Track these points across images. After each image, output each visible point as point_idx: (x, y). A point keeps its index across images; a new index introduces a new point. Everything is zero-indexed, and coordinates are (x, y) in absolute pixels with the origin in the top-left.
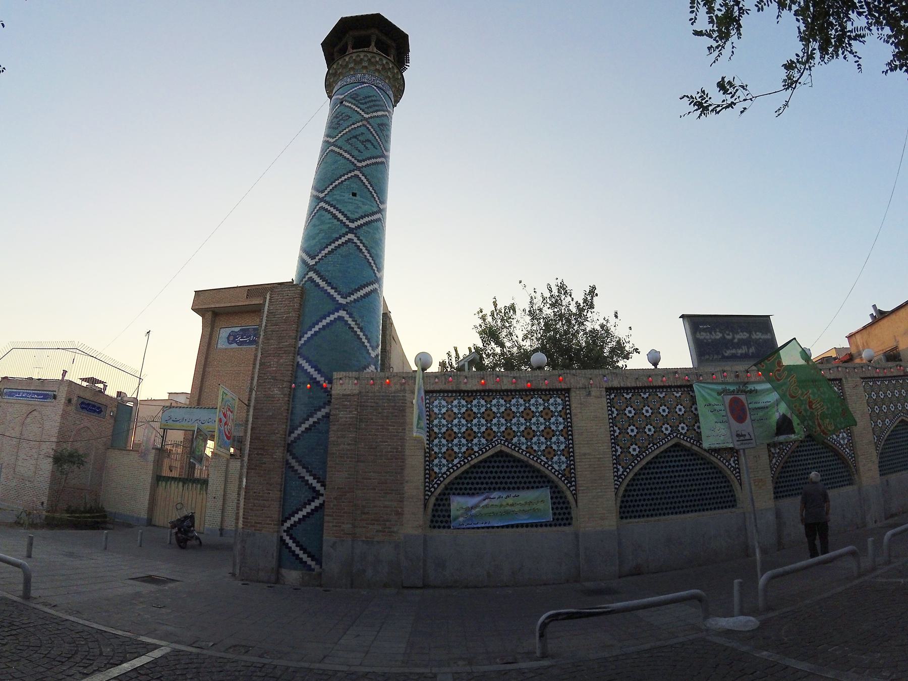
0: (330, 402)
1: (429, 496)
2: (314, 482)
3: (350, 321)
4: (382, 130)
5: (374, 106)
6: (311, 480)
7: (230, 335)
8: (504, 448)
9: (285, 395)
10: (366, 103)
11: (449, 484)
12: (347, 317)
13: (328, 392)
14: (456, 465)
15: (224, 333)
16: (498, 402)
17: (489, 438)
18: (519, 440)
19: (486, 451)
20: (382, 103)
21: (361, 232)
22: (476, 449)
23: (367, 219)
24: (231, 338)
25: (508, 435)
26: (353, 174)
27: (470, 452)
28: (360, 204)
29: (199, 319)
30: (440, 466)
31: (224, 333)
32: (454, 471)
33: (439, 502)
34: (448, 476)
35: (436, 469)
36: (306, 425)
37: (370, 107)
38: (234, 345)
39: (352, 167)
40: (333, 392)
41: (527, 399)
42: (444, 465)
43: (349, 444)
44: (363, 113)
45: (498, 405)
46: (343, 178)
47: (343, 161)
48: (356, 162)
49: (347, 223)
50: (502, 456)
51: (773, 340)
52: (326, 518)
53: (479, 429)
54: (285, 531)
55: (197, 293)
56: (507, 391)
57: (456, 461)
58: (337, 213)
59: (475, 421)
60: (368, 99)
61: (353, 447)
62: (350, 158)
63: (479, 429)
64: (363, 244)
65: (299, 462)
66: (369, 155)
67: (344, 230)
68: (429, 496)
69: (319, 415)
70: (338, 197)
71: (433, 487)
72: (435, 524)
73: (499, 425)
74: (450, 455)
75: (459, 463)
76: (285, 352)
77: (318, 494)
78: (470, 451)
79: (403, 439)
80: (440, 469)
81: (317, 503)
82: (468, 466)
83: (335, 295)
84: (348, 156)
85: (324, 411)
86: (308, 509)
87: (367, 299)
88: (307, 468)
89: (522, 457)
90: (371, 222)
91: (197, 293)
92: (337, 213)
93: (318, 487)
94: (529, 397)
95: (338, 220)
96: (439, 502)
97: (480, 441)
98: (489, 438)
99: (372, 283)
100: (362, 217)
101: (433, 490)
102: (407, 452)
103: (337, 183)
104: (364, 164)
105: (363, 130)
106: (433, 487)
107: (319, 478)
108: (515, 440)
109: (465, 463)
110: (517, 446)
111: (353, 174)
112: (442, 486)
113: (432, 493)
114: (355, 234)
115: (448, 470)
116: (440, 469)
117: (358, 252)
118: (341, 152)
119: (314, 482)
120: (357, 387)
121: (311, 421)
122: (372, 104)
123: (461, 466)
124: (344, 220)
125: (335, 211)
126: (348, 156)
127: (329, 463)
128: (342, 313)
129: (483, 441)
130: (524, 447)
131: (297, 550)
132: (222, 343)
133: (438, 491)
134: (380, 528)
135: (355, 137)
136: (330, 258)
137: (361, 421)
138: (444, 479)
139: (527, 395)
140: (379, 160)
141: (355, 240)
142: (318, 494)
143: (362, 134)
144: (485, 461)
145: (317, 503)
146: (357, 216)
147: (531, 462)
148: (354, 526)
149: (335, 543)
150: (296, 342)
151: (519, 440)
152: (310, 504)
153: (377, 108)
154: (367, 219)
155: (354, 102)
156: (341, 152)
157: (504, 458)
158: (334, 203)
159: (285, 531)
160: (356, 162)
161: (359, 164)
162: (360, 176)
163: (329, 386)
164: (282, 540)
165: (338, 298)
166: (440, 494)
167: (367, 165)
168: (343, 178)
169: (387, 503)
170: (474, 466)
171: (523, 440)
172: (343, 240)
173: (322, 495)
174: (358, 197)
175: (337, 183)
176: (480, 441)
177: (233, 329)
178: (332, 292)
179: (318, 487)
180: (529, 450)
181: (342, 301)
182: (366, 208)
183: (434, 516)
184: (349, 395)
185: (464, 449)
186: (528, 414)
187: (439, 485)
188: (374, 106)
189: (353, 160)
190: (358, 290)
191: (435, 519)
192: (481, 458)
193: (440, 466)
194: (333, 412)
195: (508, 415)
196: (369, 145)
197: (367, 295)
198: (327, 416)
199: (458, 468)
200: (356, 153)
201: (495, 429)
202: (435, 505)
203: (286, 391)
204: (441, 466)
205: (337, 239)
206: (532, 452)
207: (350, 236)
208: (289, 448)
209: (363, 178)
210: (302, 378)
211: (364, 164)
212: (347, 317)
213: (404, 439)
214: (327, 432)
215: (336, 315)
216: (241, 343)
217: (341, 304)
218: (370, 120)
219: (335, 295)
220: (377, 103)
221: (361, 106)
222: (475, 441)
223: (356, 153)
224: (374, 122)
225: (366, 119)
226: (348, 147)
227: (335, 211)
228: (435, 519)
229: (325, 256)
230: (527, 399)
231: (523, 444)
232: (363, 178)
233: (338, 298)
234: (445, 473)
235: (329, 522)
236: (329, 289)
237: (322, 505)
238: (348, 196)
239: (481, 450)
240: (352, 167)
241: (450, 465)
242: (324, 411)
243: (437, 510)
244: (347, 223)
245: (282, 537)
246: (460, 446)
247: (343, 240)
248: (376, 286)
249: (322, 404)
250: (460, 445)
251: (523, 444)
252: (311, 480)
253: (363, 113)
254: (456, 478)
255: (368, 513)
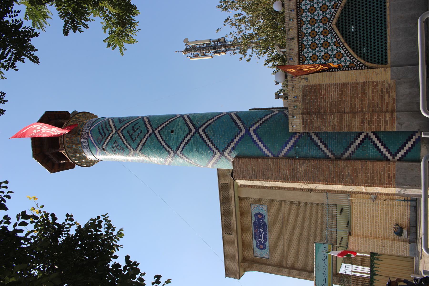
0: (308, 133)
1: (365, 66)
2: (360, 139)
3: (256, 125)
4: (124, 121)
5: (106, 127)
6: (358, 142)
7: (259, 248)
8: (334, 23)
9: (304, 163)
10: (104, 133)
11: (357, 55)
12: (254, 128)
13: (302, 135)
14: (345, 52)
15: (258, 252)
16: (305, 29)
17: (328, 32)
18: (328, 14)
19: (336, 33)
20: (100, 125)
21: (198, 125)
22: (334, 40)
23: (189, 122)
24: (261, 247)
25: (325, 21)
26: (158, 134)
27: (337, 44)
28: (179, 127)
29: (248, 275)
30: (345, 61)
31: (258, 252)
32: (349, 52)
33: (369, 60)
34: (352, 56)
35: (348, 63)
36: (323, 147)
37: (107, 130)
38: (267, 244)
39: (153, 135)
40: (302, 131)
41: (302, 11)
42: (345, 59)
43: (334, 119)
44: (112, 133)
45: (307, 29)
46: (161, 140)
47: (148, 142)
48: (149, 133)
49: (192, 134)
50: (339, 24)
51: (348, 263)
52: (383, 130)
53: (322, 39)
54: (393, 158)
55: (227, 275)
56: (298, 24)
57: (342, 52)
58: (185, 141)
59: (317, 42)
60: (101, 131)
61: (336, 116)
62: (146, 137)
63: (322, 39)
64: (203, 124)
65: (346, 150)
66: (144, 126)
67: (197, 135)
68: (365, 66)
69: (316, 139)
70: (174, 142)
71: (359, 64)
72: (384, 62)
73: (319, 27)
74: (339, 56)
75: (343, 50)
76: (277, 165)
77: (367, 136)
78: (336, 44)
79: (329, 85)
80: (348, 61)
81: (373, 137)
82: (345, 44)
83: (240, 136)
84: (145, 139)
85: (314, 136)
86: (377, 142)
87: (242, 118)
88: (350, 145)
89: (339, 11)
90: (190, 120)
91: (227, 275)
92: (185, 141)
93: (362, 137)
94: (301, 10)
95: (190, 140)
96: (369, 60)
97: (329, 38)
98: (328, 32)
99: (231, 116)
100: (188, 125)
101: (361, 65)
102: (338, 82)
103: (164, 144)
104: (150, 128)
105: (125, 132)
106: (359, 64)
107: (357, 136)
108: (328, 16)
109: (344, 46)
110: (332, 15)
111: (158, 134)
112: (359, 59)
113: (363, 65)
114: (199, 128)
115: (348, 56)
116: (348, 61)
117: (211, 125)
118: (141, 144)
119: (360, 139)
120: (298, 116)
121: (320, 144)
122: (105, 129)
123: (345, 48)
124: (190, 136)
125: (184, 143)
126: (145, 139)
127: (347, 130)
128: (251, 131)
129: (329, 36)
130: (333, 10)
131: (406, 148)
132: (265, 254)
133: (363, 61)
134: (387, 95)
135: (131, 136)
136: (215, 142)
137: (319, 112)
138: (354, 58)
139: (300, 11)
140: (111, 123)
141: (203, 127)
142: (367, 136)
143: (128, 132)
144: (342, 34)
145: (373, 137)
146: (187, 128)
147: (342, 5)
148: (387, 111)
149: (399, 123)
150: (271, 158)
151: (328, 14)
152: (374, 141)
153: (108, 126)
154: (189, 122)
155: (103, 140)
156: (141, 144)
157: (340, 22)
158: (178, 144)
159: (393, 158)
160: (149, 133)
161: (151, 131)
162: (159, 129)
163: (298, 134)
164: (400, 160)
165: (241, 134)
166: (364, 60)
167: (151, 126)
168: (161, 140)
169: (371, 92)
170: (346, 41)
171: (328, 11)
172: (203, 135)
173: (367, 134)
174: (174, 129)
175: (164, 144)
176: (329, 38)
177: (255, 245)
178: (238, 138)
179: (362, 137)
180: (334, 7)
181: (243, 132)
182: (181, 123)
183: (378, 63)
184: (303, 120)
185: (335, 47)
186: (312, 10)
187: (358, 61)
188: (106, 127)
189: (147, 135)
190: (236, 123)
191: (381, 62)
192: (340, 36)
193: (345, 61)
194: (314, 130)
195: (313, 22)
196: (136, 127)
197: (238, 117)
198: (317, 134)
199: (347, 50)
200: (142, 134)
201: (321, 29)
202: (371, 63)
203: (301, 161)
204: (346, 61)
205: (203, 139)
206: (336, 4)
207: (201, 131)
208: (338, 158)
209: (160, 128)
210: (292, 153)
211: (150, 128)
212: (254, 128)
213: (329, 84)
214: (327, 133)
215: (252, 134)
216: (265, 238)
217: (245, 132)
218: (117, 129)
219: (240, 136)
220: (104, 125)
221: (107, 135)
222: (329, 41)
223: (142, 134)
224: (118, 126)
225: (117, 131)
226: (138, 140)
227: (184, 143)
228: (381, 62)
229: (214, 145)
230: (302, 11)
231: (330, 11)
232: (160, 128)
233: (241, 134)
234: (350, 58)
235: (385, 128)
236: (236, 140)
237: (374, 133)
238: (173, 136)
239: (335, 37)
240: (153, 135)
241: (345, 55)
242: (314, 136)
243: (375, 61)
244: (192, 134)
245: (398, 160)
246: (333, 50)
247: (203, 135)
248: (232, 114)
249: (309, 138)
250: (332, 50)
251: (330, 11)
252: (358, 142)
253: (112, 133)
254: (354, 51)
255: (378, 104)
